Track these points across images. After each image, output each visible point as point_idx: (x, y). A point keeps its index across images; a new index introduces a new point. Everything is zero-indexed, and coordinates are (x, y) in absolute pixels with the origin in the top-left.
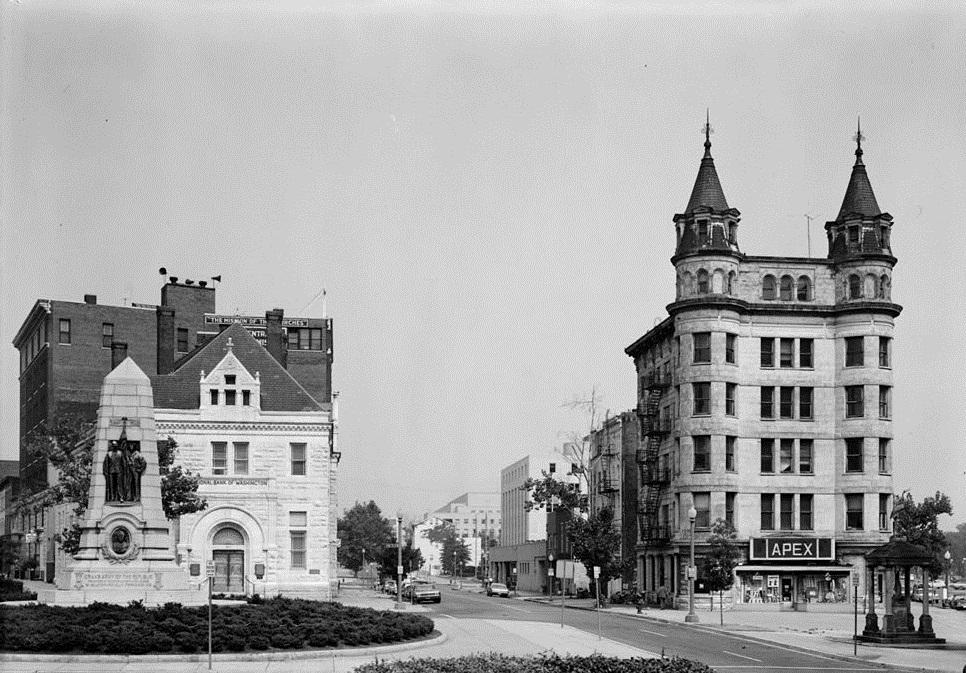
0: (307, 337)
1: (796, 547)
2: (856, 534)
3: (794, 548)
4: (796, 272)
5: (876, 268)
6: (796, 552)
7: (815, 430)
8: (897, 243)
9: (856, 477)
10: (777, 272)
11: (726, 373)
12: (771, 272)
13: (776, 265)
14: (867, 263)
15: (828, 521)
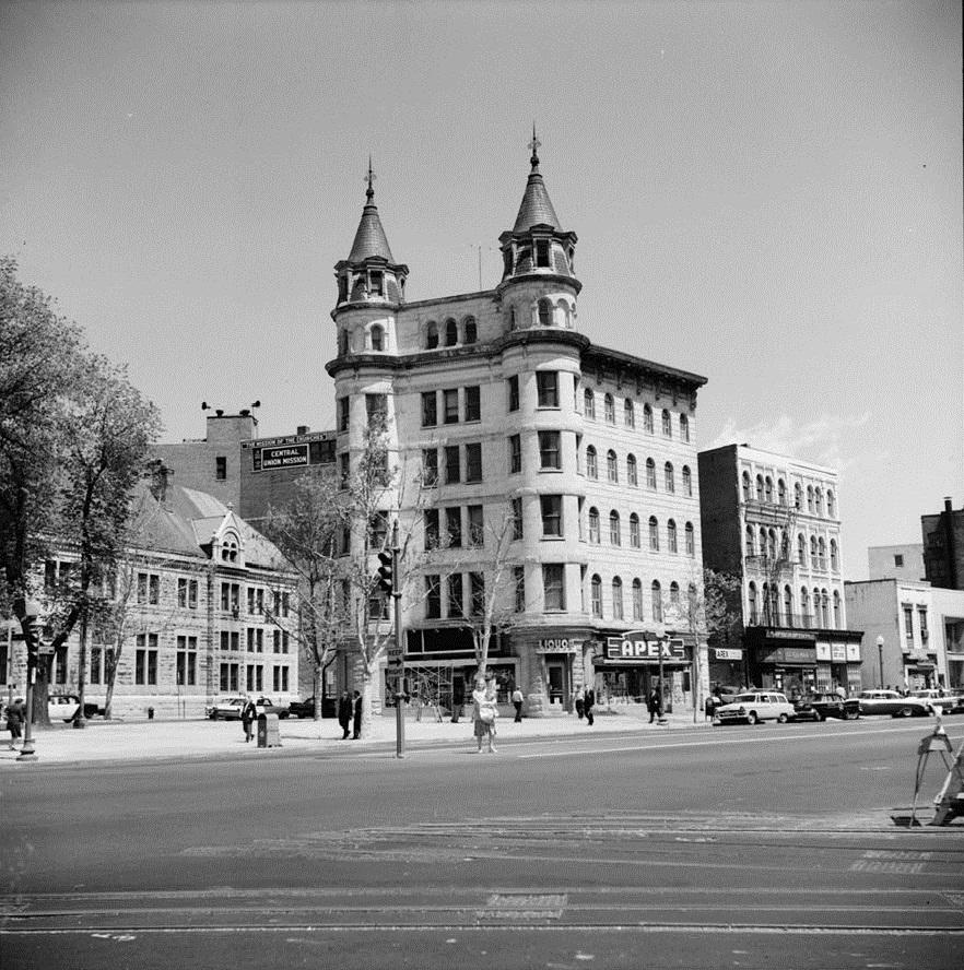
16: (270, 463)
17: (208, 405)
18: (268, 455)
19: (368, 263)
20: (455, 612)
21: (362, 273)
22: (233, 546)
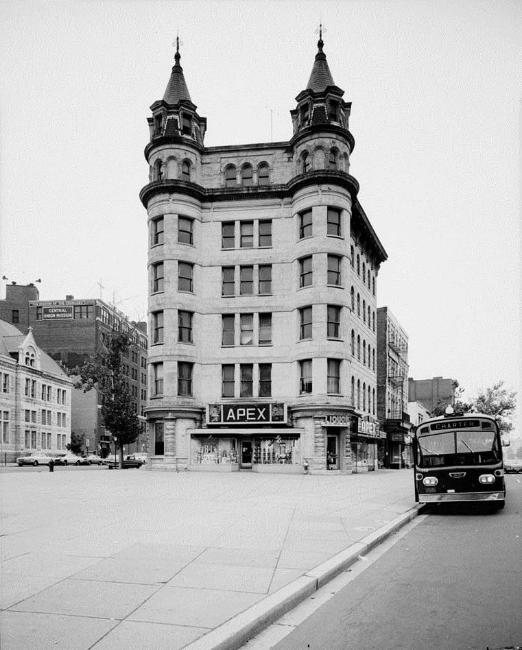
0: (86, 311)
1: (250, 412)
2: (307, 399)
3: (247, 413)
4: (255, 159)
5: (324, 140)
6: (250, 416)
7: (273, 304)
8: (355, 125)
9: (306, 343)
10: (237, 161)
11: (178, 252)
12: (232, 161)
13: (235, 154)
14: (316, 136)
15: (285, 389)
16: (48, 316)
17: (6, 277)
18: (46, 311)
19: (181, 105)
20: (248, 391)
21: (175, 121)
22: (32, 355)
